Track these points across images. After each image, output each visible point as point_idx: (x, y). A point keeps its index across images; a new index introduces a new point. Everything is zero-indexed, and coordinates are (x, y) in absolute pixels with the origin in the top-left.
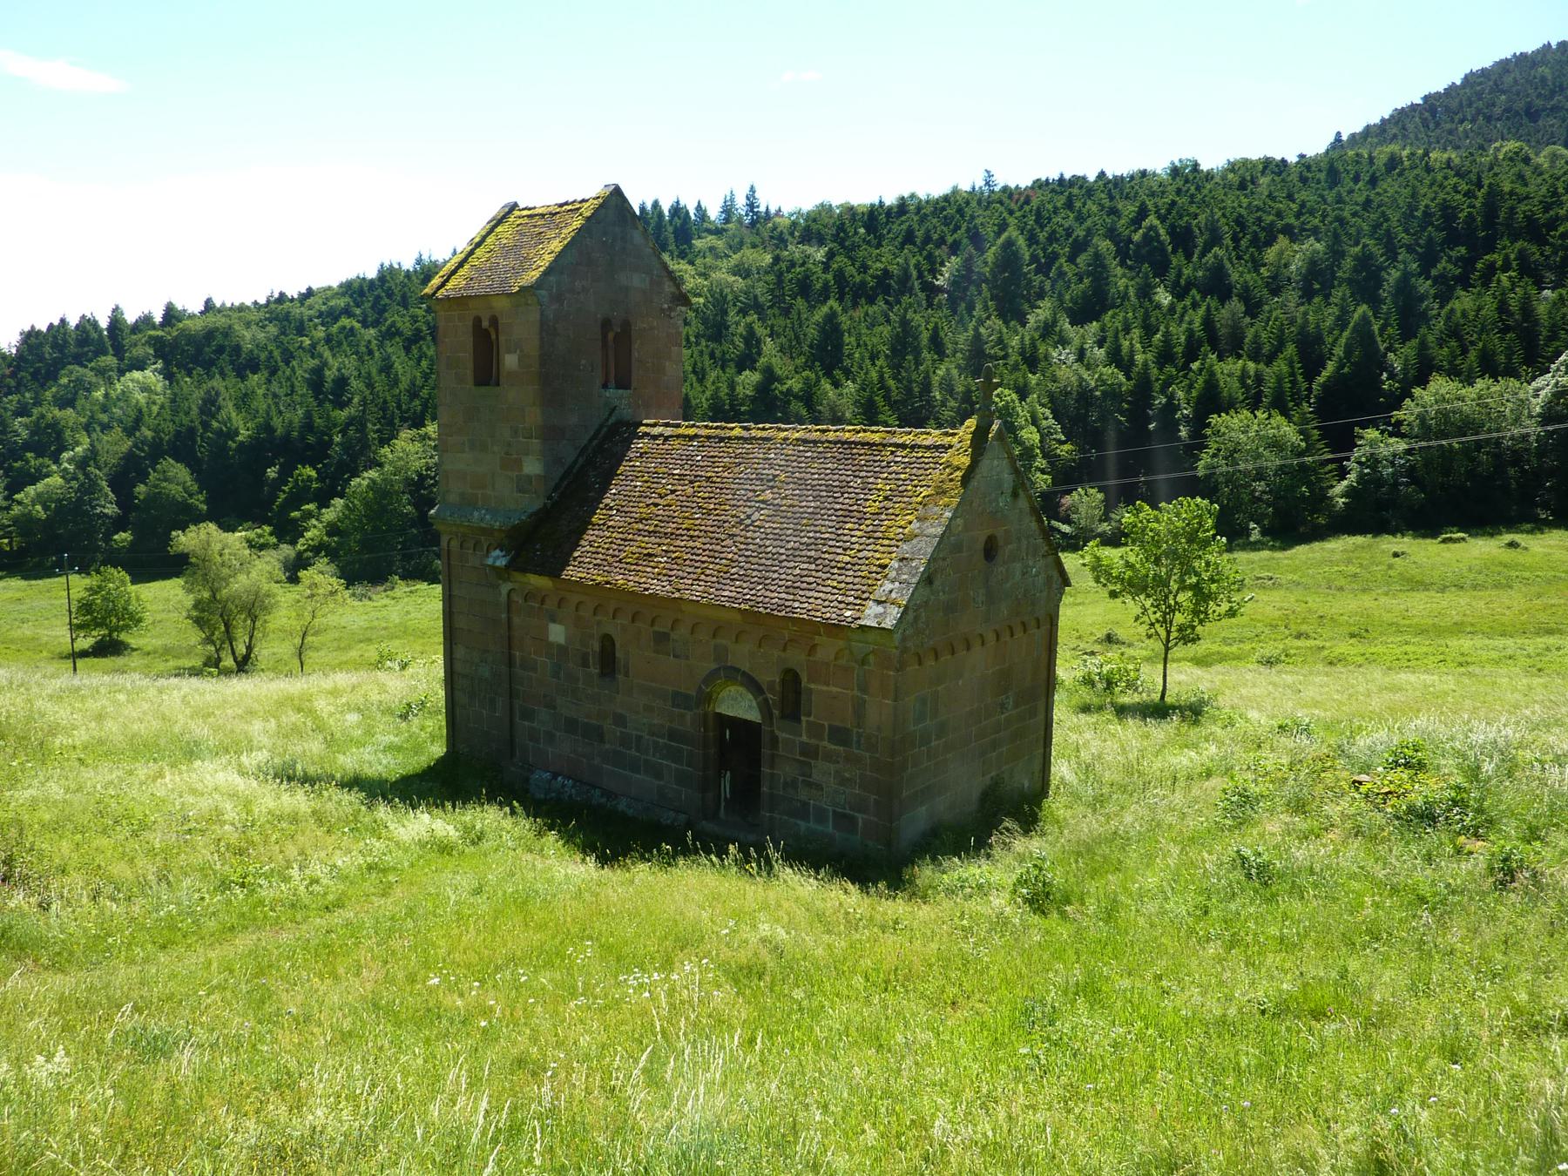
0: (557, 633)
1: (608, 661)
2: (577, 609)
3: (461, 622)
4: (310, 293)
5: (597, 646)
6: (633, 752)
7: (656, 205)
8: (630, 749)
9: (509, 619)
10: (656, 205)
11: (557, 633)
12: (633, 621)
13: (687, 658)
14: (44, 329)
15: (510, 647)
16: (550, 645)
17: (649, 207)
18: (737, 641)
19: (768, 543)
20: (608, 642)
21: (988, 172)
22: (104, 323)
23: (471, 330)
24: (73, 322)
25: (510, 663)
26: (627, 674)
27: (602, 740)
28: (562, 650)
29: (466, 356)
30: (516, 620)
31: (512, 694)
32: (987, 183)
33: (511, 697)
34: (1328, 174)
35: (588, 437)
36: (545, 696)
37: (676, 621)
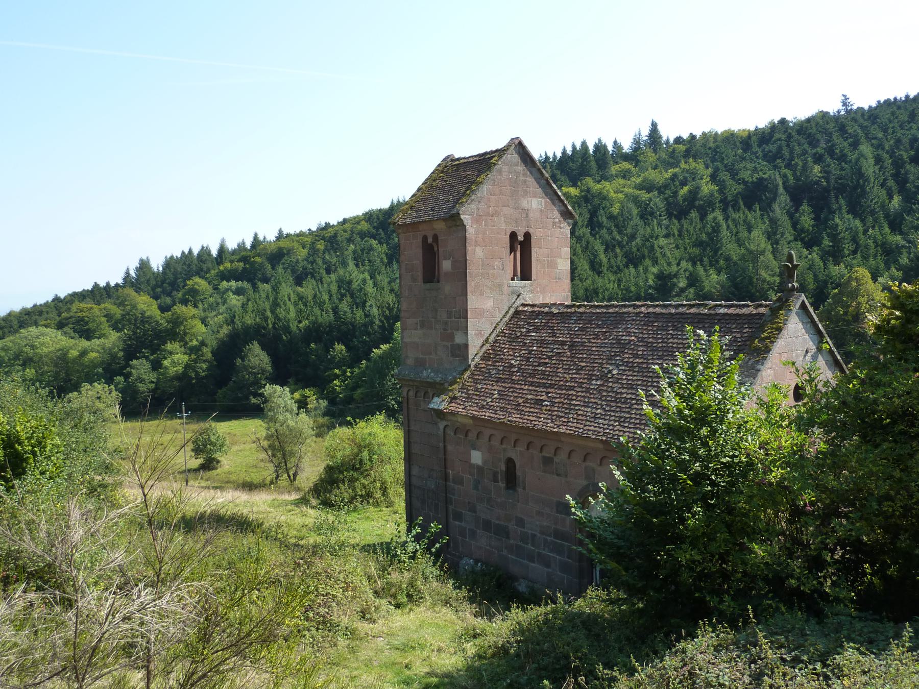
0: (476, 457)
1: (511, 477)
2: (490, 441)
3: (416, 449)
4: (345, 221)
5: (503, 468)
6: (529, 546)
7: (584, 144)
8: (527, 544)
9: (445, 447)
10: (584, 144)
11: (476, 457)
12: (528, 449)
13: (566, 476)
14: (236, 247)
15: (445, 468)
16: (472, 466)
17: (578, 147)
18: (601, 464)
19: (624, 391)
20: (510, 463)
21: (844, 96)
22: (214, 253)
23: (421, 244)
24: (196, 252)
25: (446, 478)
26: (524, 488)
27: (508, 537)
28: (480, 469)
29: (418, 263)
30: (450, 448)
31: (447, 501)
32: (844, 104)
33: (446, 504)
34: (361, 373)
35: (501, 316)
36: (469, 503)
37: (557, 449)
